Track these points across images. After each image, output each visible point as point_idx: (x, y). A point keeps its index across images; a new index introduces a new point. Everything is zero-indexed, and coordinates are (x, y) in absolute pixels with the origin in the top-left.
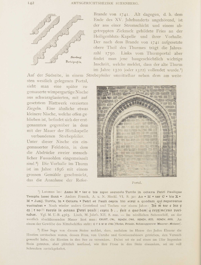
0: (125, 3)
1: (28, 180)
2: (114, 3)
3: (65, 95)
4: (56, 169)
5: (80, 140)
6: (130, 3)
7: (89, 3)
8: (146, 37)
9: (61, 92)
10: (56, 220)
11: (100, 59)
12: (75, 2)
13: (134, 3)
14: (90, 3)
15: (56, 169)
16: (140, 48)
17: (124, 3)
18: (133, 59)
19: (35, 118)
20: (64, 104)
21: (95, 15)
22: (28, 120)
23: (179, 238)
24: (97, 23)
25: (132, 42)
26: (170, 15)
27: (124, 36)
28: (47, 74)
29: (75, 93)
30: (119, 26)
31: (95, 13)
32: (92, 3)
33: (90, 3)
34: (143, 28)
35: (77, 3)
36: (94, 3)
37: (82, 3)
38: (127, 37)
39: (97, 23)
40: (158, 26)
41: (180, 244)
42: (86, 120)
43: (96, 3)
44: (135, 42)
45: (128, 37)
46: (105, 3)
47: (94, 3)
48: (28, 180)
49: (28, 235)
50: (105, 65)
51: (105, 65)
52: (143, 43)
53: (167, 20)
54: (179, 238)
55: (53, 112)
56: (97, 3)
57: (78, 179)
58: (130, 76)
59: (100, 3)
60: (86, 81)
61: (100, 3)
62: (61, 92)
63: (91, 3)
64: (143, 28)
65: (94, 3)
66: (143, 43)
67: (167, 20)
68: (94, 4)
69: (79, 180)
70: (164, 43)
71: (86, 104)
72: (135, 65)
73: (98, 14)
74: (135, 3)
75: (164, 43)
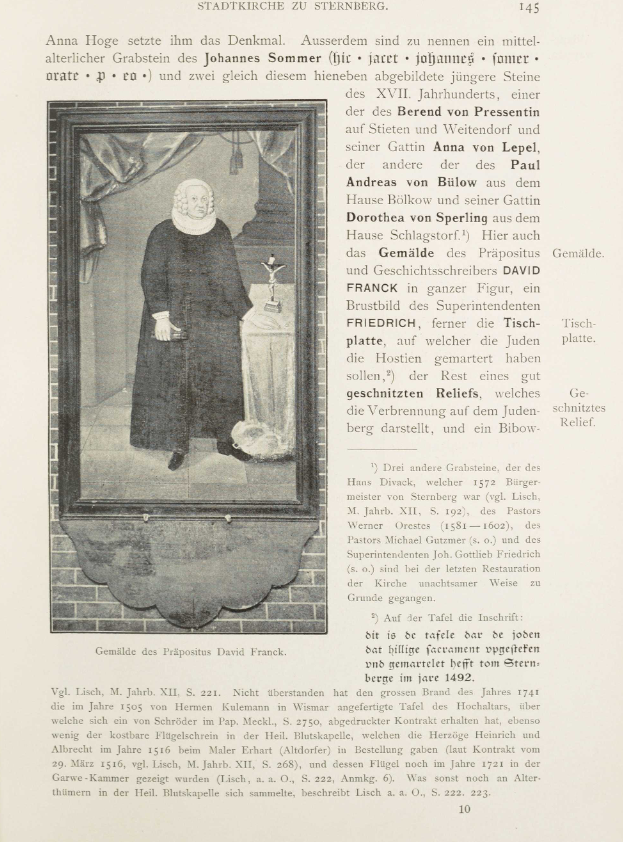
1: (349, 254)
16: (302, 750)
17: (340, 7)
18: (351, 429)
20: (450, 722)
23: (532, 562)
25: (389, 166)
26: (189, 692)
28: (440, 303)
30: (359, 113)
31: (392, 197)
40: (536, 131)
41: (538, 584)
42: (536, 750)
44: (401, 166)
48: (349, 254)
52: (453, 114)
53: (401, 412)
54: (532, 562)
55: (459, 333)
57: (445, 373)
67: (401, 412)
69: (449, 376)
70: (456, 412)
74: (258, 6)
75: (456, 412)
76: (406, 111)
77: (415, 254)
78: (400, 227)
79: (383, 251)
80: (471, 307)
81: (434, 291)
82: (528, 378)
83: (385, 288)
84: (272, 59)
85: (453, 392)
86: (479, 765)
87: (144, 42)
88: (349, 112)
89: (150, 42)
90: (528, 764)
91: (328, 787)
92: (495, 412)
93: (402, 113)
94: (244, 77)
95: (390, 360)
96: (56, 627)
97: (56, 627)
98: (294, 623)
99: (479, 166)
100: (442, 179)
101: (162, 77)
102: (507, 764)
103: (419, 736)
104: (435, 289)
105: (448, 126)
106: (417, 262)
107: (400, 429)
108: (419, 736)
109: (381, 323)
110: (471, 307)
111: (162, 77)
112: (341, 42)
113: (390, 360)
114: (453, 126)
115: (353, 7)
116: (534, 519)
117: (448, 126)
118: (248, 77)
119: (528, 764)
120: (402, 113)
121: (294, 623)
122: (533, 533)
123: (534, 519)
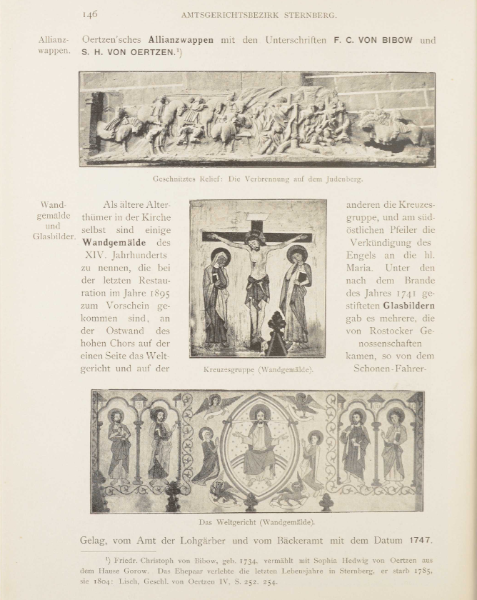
0: (305, 16)
4: (154, 293)
5: (366, 337)
6: (317, 15)
7: (222, 15)
10: (378, 344)
13: (325, 16)
15: (154, 293)
21: (408, 282)
24: (355, 288)
25: (420, 281)
27: (148, 217)
29: (357, 241)
31: (408, 278)
32: (229, 15)
33: (226, 15)
34: (365, 225)
36: (234, 15)
37: (208, 15)
39: (355, 288)
43: (238, 15)
46: (259, 15)
56: (199, 15)
58: (96, 231)
59: (248, 14)
61: (248, 14)
64: (365, 225)
65: (234, 14)
68: (234, 16)
69: (145, 281)
71: (417, 345)
72: (63, 216)
73: (414, 281)
77: (132, 244)
78: (132, 566)
81: (202, 543)
83: (401, 40)
84: (108, 357)
85: (161, 354)
88: (84, 281)
90: (161, 344)
92: (366, 541)
96: (433, 75)
97: (433, 75)
98: (379, 94)
99: (159, 344)
101: (118, 369)
105: (149, 354)
106: (135, 249)
111: (118, 369)
114: (153, 354)
115: (312, 16)
117: (149, 354)
118: (367, 231)
119: (161, 344)
121: (379, 94)
122: (164, 338)
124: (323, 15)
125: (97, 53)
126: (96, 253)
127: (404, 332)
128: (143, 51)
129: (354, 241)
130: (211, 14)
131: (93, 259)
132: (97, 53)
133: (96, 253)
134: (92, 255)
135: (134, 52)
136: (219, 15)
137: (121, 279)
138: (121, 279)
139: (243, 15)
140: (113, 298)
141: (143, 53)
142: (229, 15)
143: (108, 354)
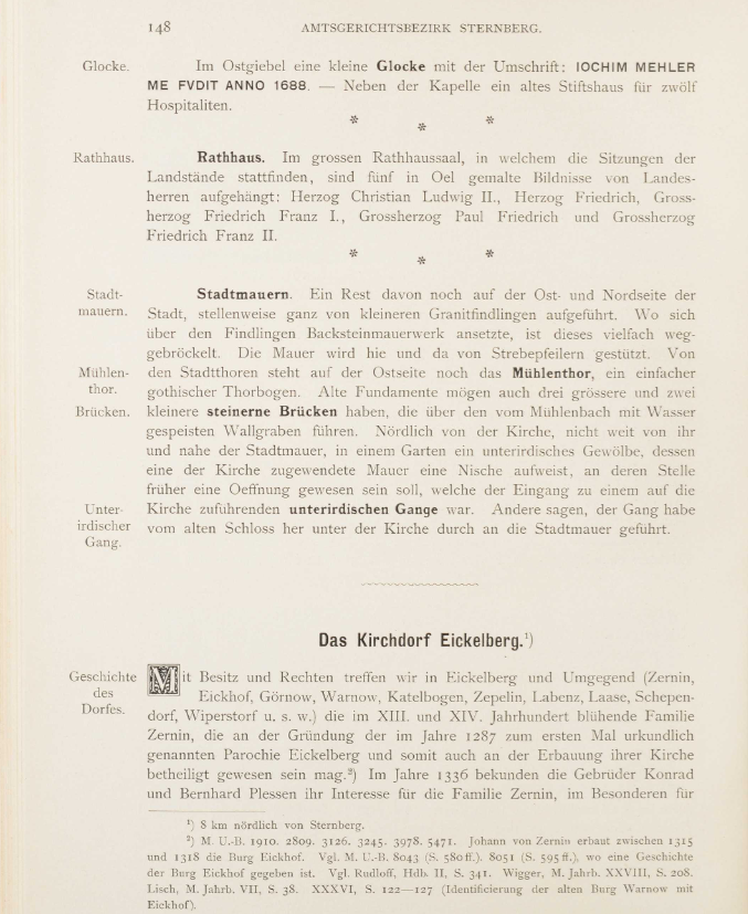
2: (455, 28)
3: (663, 727)
6: (512, 28)
8: (631, 679)
9: (350, 757)
11: (168, 490)
12: (315, 25)
13: (524, 29)
14: (369, 28)
19: (658, 693)
22: (582, 718)
27: (439, 85)
29: (678, 352)
33: (369, 28)
35: (322, 28)
36: (383, 28)
38: (449, 88)
43: (388, 28)
45: (454, 87)
46: (420, 28)
47: (383, 28)
49: (521, 199)
50: (544, 68)
51: (544, 68)
52: (612, 181)
56: (328, 28)
60: (612, 737)
61: (403, 27)
62: (350, 757)
63: (374, 28)
66: (612, 181)
68: (382, 30)
74: (528, 29)
76: (289, 410)
79: (400, 508)
80: (516, 453)
81: (543, 493)
82: (155, 395)
86: (461, 737)
87: (490, 335)
89: (497, 335)
91: (556, 403)
93: (285, 413)
94: (543, 219)
95: (164, 106)
100: (285, 408)
102: (427, 353)
103: (412, 413)
104: (545, 491)
107: (225, 717)
108: (412, 413)
109: (200, 85)
110: (516, 453)
112: (627, 297)
113: (164, 106)
115: (503, 30)
116: (688, 423)
120: (285, 413)
123: (688, 423)
124: (520, 28)
125: (605, 65)
126: (467, 714)
127: (318, 756)
128: (685, 66)
129: (673, 350)
130: (346, 27)
131: (461, 723)
132: (605, 65)
133: (467, 714)
134: (460, 716)
135: (260, 85)
136: (358, 28)
137: (334, 526)
138: (334, 526)
139: (395, 28)
140: (227, 459)
141: (686, 68)
142: (374, 28)
143: (229, 525)
